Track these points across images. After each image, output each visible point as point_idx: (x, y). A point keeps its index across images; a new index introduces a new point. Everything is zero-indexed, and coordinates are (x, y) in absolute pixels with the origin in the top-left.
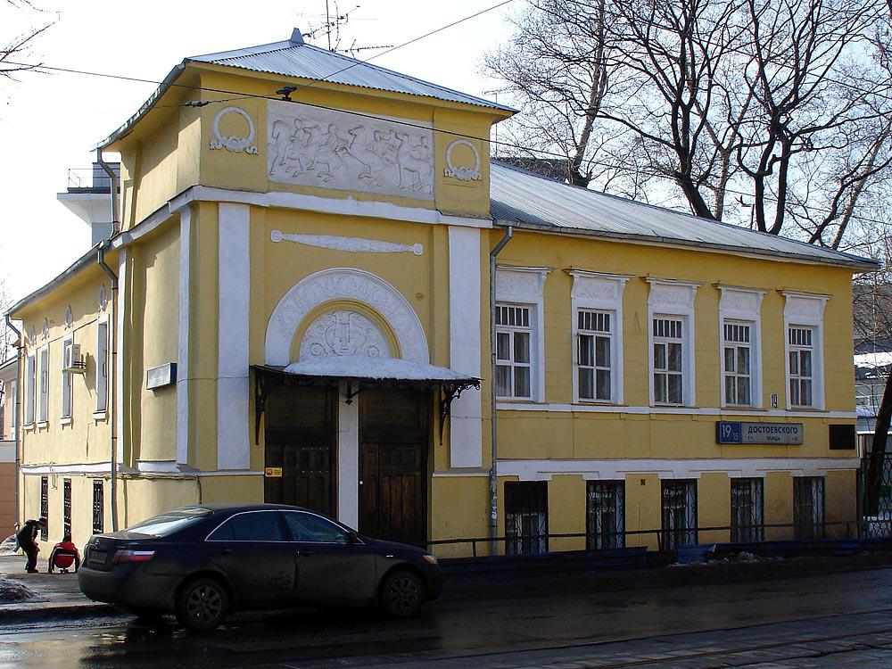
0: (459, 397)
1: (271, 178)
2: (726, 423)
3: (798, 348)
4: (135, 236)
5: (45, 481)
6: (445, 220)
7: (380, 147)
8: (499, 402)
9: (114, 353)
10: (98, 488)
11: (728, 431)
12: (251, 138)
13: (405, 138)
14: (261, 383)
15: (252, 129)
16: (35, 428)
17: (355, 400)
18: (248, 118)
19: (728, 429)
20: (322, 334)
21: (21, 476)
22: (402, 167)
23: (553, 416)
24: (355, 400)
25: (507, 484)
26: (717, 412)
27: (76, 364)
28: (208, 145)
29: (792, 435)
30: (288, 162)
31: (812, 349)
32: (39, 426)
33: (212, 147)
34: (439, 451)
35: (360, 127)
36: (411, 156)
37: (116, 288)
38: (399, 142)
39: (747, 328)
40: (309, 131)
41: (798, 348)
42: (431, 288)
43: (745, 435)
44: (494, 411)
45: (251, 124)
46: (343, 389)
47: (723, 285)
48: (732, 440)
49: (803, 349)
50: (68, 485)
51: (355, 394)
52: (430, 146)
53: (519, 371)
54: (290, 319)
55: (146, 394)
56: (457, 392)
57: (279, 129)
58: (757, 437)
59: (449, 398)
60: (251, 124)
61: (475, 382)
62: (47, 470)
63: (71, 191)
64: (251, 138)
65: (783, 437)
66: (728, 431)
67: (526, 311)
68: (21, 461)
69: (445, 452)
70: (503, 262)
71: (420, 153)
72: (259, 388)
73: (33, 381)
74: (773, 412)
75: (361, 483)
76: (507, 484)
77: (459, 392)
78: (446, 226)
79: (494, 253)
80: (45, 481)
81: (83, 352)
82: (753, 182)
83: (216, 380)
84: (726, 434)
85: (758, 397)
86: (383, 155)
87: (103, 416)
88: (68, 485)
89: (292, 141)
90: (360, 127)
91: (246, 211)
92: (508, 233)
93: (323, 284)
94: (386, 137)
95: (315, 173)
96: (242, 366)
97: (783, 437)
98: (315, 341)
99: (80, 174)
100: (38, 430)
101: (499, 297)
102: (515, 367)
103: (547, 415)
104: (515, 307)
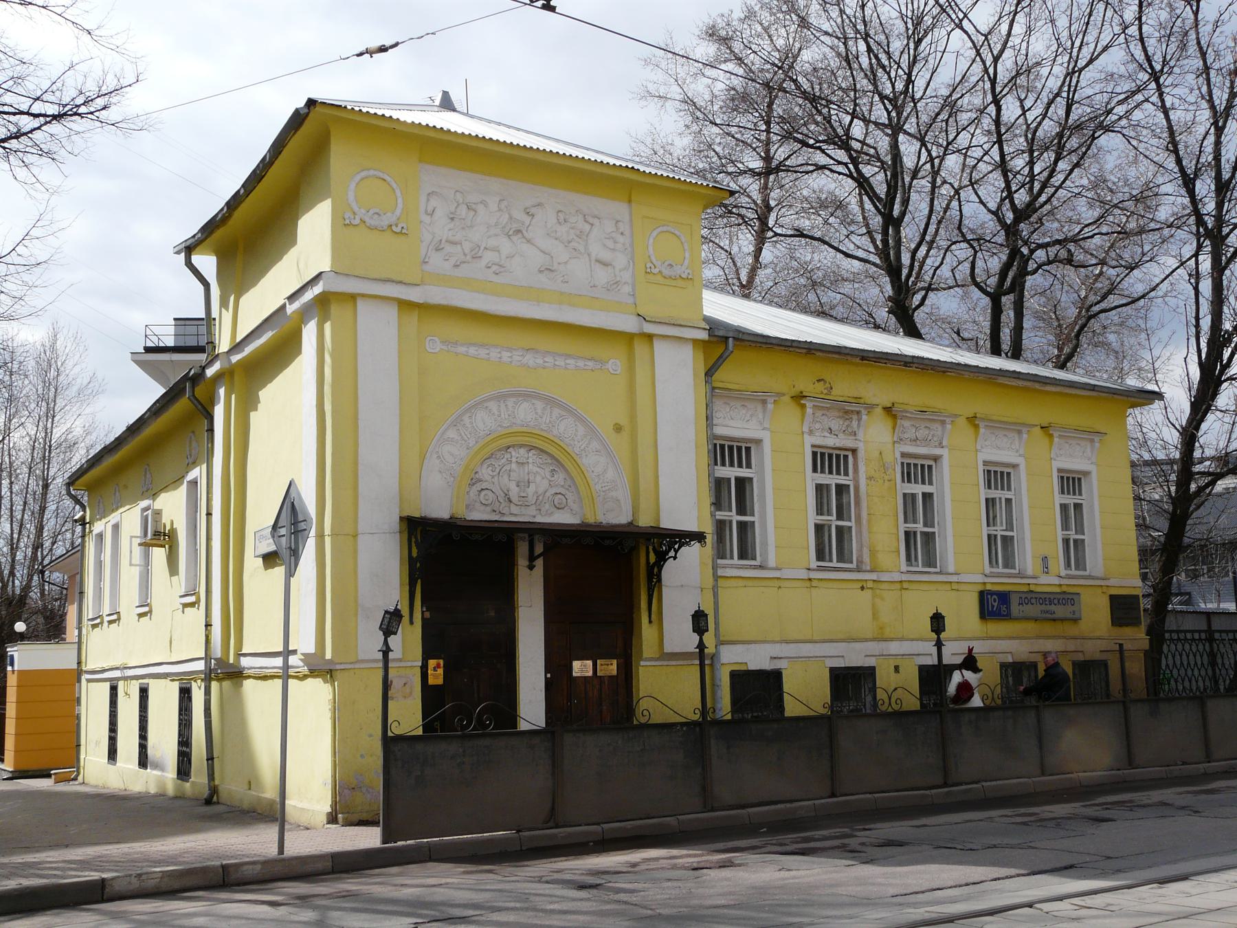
0: (675, 558)
1: (427, 268)
2: (991, 593)
3: (1070, 500)
4: (235, 358)
5: (114, 690)
6: (649, 328)
7: (563, 230)
8: (724, 567)
9: (209, 514)
10: (185, 694)
11: (994, 603)
12: (398, 212)
13: (596, 221)
14: (416, 538)
15: (400, 201)
16: (102, 623)
17: (539, 563)
18: (395, 186)
19: (995, 601)
20: (493, 477)
21: (84, 682)
22: (593, 258)
23: (787, 584)
24: (539, 563)
25: (733, 675)
26: (980, 579)
27: (157, 534)
28: (342, 224)
29: (1070, 608)
30: (449, 248)
31: (1083, 499)
32: (106, 619)
33: (347, 222)
34: (647, 632)
35: (539, 205)
36: (605, 245)
37: (211, 430)
38: (587, 227)
39: (1009, 474)
40: (474, 206)
41: (1070, 500)
42: (633, 417)
43: (1015, 609)
44: (716, 577)
45: (399, 194)
46: (522, 549)
47: (982, 419)
48: (1000, 615)
49: (1076, 501)
50: (144, 692)
51: (539, 556)
52: (627, 233)
53: (743, 526)
54: (452, 455)
55: (253, 563)
56: (672, 553)
57: (434, 202)
58: (1031, 610)
59: (662, 558)
60: (399, 194)
61: (699, 537)
62: (117, 674)
63: (148, 350)
64: (398, 212)
65: (1060, 611)
66: (994, 603)
67: (748, 449)
68: (83, 665)
69: (656, 634)
70: (720, 385)
71: (615, 242)
72: (413, 544)
73: (99, 564)
74: (1044, 579)
75: (549, 675)
76: (733, 675)
77: (676, 551)
78: (650, 337)
79: (709, 373)
80: (114, 690)
81: (166, 520)
82: (986, 301)
83: (355, 536)
84: (993, 606)
85: (1027, 560)
86: (569, 242)
87: (192, 599)
88: (144, 692)
89: (452, 219)
90: (539, 205)
91: (392, 312)
92: (726, 348)
93: (495, 410)
94: (573, 220)
95: (483, 263)
96: (390, 520)
97: (1060, 611)
98: (484, 485)
99: (157, 330)
100: (106, 624)
101: (719, 431)
102: (737, 522)
103: (777, 583)
104: (735, 444)
